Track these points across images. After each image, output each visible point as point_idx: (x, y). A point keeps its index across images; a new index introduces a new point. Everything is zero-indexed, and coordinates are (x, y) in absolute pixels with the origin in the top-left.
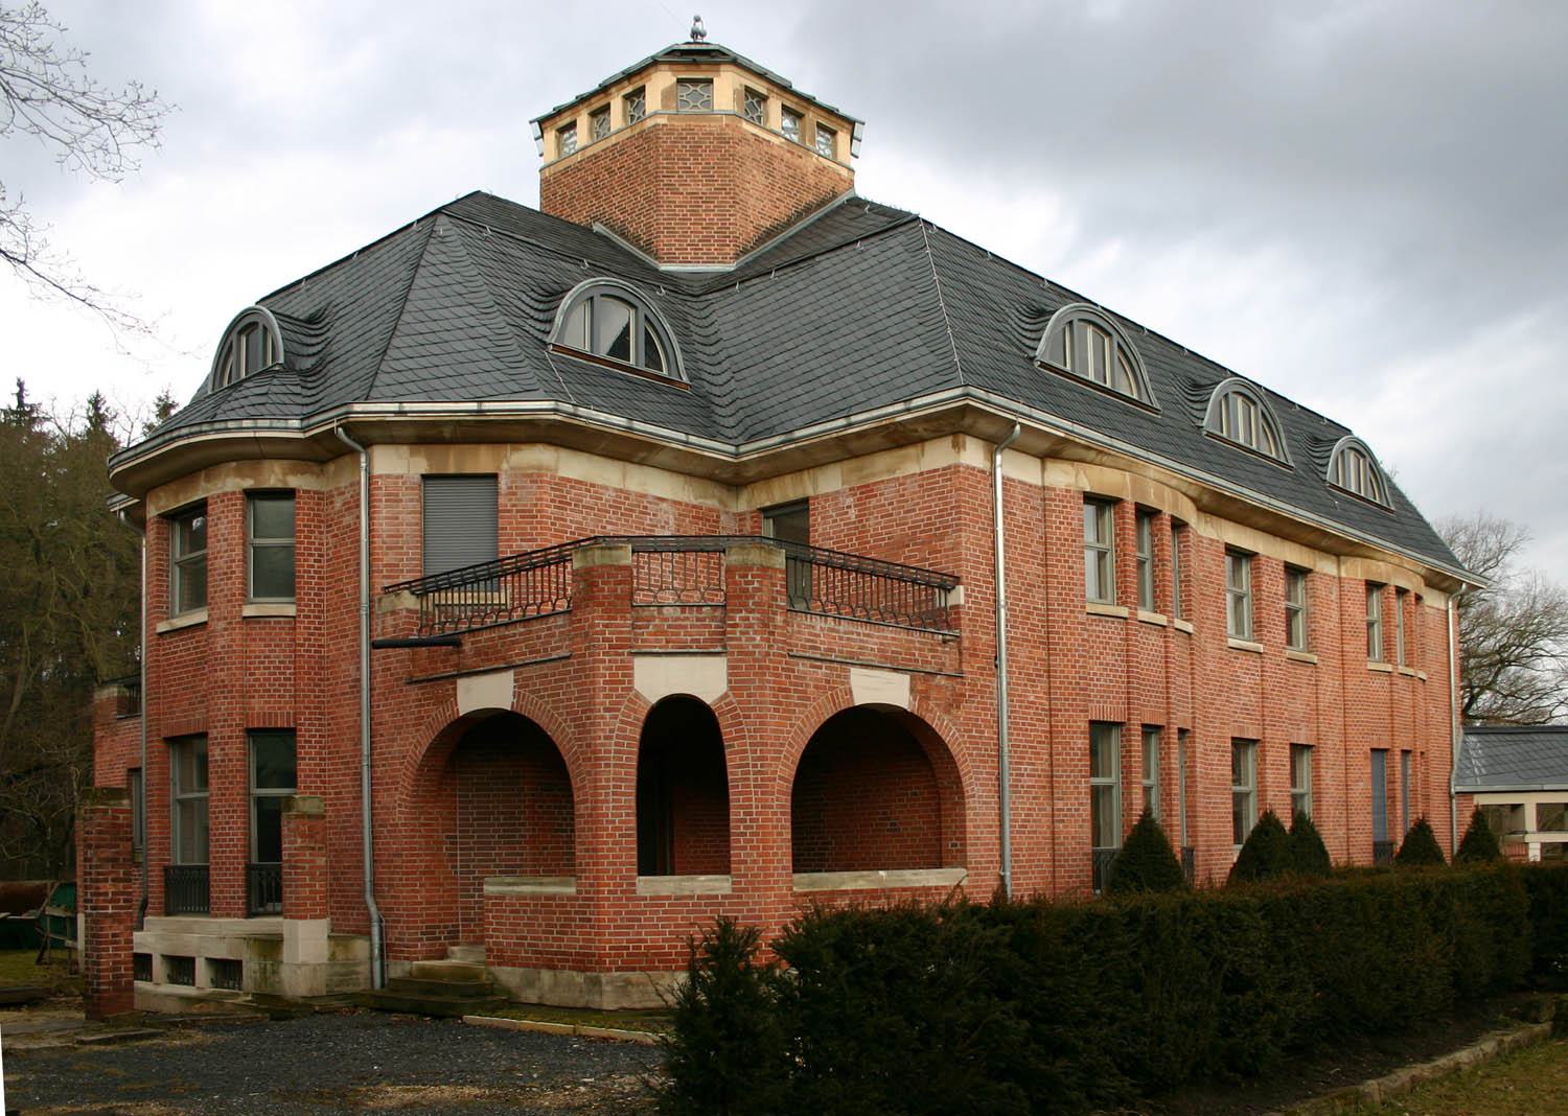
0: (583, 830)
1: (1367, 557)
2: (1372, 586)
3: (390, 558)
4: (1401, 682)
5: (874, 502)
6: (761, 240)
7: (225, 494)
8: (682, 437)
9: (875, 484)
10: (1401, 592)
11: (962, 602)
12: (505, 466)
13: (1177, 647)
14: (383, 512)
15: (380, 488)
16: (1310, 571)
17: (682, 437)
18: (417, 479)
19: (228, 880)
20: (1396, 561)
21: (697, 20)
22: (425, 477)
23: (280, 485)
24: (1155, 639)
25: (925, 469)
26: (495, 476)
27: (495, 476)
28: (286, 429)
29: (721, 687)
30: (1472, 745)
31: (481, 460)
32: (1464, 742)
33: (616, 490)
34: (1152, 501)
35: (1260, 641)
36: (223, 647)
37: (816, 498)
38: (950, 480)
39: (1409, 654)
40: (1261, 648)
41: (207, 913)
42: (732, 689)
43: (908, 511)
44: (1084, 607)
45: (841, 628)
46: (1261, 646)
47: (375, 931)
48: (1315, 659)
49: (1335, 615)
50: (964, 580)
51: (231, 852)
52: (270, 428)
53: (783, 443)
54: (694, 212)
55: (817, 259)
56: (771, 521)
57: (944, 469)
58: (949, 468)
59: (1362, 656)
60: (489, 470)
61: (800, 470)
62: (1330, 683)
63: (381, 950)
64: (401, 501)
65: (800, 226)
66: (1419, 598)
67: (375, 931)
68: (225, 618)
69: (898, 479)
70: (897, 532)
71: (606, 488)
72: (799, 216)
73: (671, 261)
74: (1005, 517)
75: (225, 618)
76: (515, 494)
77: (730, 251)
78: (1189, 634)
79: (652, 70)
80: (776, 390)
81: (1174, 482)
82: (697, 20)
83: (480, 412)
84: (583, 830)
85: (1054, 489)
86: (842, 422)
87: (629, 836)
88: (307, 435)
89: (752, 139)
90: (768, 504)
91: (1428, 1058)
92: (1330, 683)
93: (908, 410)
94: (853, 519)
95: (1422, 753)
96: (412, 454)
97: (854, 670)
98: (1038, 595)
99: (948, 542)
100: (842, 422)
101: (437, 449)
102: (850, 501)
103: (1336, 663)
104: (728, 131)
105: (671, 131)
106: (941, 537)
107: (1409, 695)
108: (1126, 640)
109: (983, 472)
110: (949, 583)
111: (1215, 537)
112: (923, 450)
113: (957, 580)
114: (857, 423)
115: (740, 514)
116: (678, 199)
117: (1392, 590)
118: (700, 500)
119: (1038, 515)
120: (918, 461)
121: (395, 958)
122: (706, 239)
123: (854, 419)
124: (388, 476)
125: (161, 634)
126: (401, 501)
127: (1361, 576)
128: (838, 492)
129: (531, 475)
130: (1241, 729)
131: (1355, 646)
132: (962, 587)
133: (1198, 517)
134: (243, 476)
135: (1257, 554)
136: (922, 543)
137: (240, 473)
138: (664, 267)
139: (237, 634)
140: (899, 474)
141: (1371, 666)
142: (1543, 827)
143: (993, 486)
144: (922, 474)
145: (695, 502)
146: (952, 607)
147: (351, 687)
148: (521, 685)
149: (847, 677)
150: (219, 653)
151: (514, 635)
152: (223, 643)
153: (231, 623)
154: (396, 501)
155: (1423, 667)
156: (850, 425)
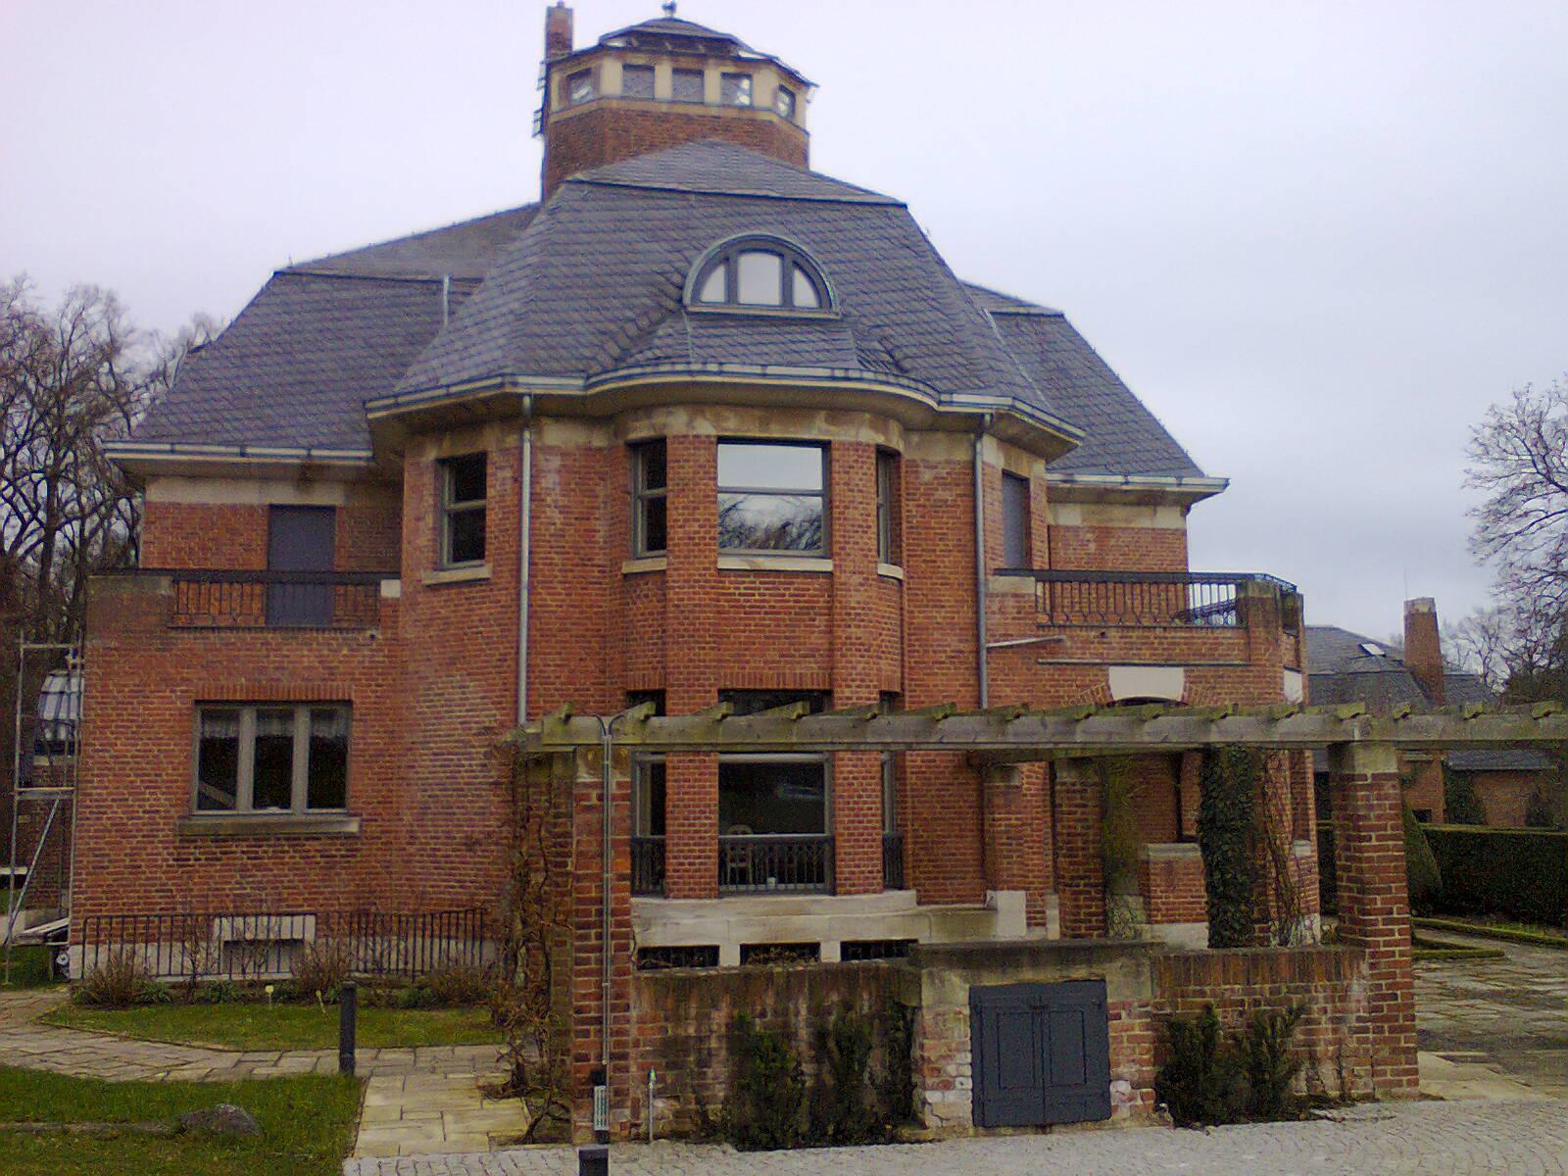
5: (1112, 542)
7: (859, 444)
19: (866, 853)
41: (663, 894)
51: (869, 822)
53: (1065, 482)
69: (1133, 529)
75: (861, 573)
79: (763, 66)
80: (502, 320)
88: (942, 409)
91: (1021, 985)
94: (1093, 551)
101: (1014, 451)
102: (1089, 536)
112: (1155, 514)
140: (1133, 525)
142: (285, 802)
148: (1191, 680)
152: (860, 599)
156: (1127, 483)
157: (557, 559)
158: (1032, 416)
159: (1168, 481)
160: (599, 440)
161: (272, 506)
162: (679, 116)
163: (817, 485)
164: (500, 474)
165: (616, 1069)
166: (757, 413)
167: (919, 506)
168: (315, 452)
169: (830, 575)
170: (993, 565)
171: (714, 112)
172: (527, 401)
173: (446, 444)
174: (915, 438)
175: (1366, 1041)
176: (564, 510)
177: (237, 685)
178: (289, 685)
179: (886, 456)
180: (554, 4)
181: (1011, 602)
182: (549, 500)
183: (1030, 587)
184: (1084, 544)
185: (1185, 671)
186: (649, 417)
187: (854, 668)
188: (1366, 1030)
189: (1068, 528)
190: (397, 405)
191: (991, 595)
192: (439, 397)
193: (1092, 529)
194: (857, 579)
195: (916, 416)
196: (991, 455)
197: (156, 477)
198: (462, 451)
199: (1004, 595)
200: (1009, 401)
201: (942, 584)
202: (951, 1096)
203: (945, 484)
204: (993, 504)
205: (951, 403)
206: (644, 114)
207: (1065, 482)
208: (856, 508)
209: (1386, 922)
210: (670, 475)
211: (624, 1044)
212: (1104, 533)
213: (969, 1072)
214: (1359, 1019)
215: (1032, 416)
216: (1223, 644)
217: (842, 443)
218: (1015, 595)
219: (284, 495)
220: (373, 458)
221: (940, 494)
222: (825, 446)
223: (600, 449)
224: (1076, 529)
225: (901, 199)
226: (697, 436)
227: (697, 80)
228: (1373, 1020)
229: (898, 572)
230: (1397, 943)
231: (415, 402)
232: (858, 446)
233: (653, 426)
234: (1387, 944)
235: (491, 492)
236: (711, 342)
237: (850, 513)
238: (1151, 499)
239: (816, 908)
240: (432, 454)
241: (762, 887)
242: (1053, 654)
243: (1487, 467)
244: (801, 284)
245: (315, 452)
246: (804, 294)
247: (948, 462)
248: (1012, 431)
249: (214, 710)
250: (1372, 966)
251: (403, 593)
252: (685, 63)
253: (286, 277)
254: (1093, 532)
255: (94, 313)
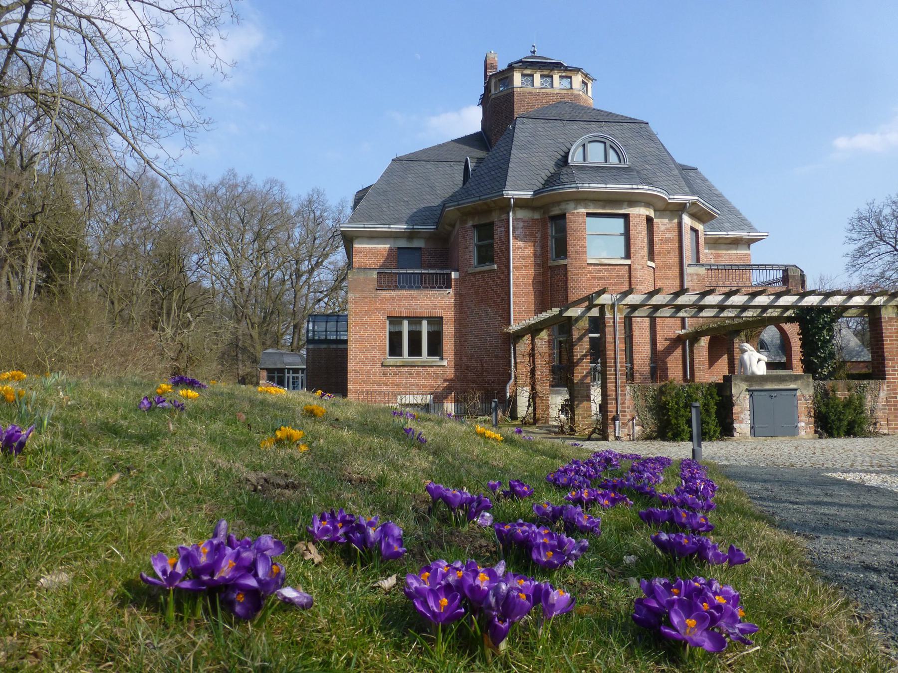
158: (703, 204)
159: (744, 234)
160: (537, 216)
161: (398, 248)
163: (622, 231)
164: (500, 229)
165: (622, 415)
166: (601, 203)
168: (415, 227)
169: (630, 266)
170: (688, 263)
171: (557, 91)
173: (476, 219)
174: (658, 213)
175: (885, 413)
177: (402, 311)
178: (419, 311)
179: (649, 220)
183: (702, 271)
186: (559, 206)
188: (885, 409)
190: (459, 205)
191: (687, 274)
192: (476, 201)
194: (640, 267)
195: (660, 205)
196: (687, 220)
197: (357, 237)
198: (483, 222)
199: (693, 274)
200: (696, 198)
202: (743, 426)
204: (687, 237)
206: (530, 93)
209: (892, 371)
211: (625, 407)
213: (749, 417)
214: (883, 405)
215: (703, 204)
217: (634, 214)
218: (696, 274)
219: (403, 244)
220: (437, 229)
222: (626, 217)
223: (537, 219)
225: (646, 121)
227: (549, 80)
228: (887, 405)
229: (653, 264)
231: (467, 203)
233: (561, 209)
234: (893, 378)
235: (496, 237)
238: (736, 242)
240: (470, 223)
243: (855, 235)
244: (611, 153)
245: (415, 227)
246: (613, 158)
248: (695, 210)
249: (394, 320)
250: (888, 386)
251: (460, 276)
252: (546, 72)
253: (396, 160)
255: (275, 190)
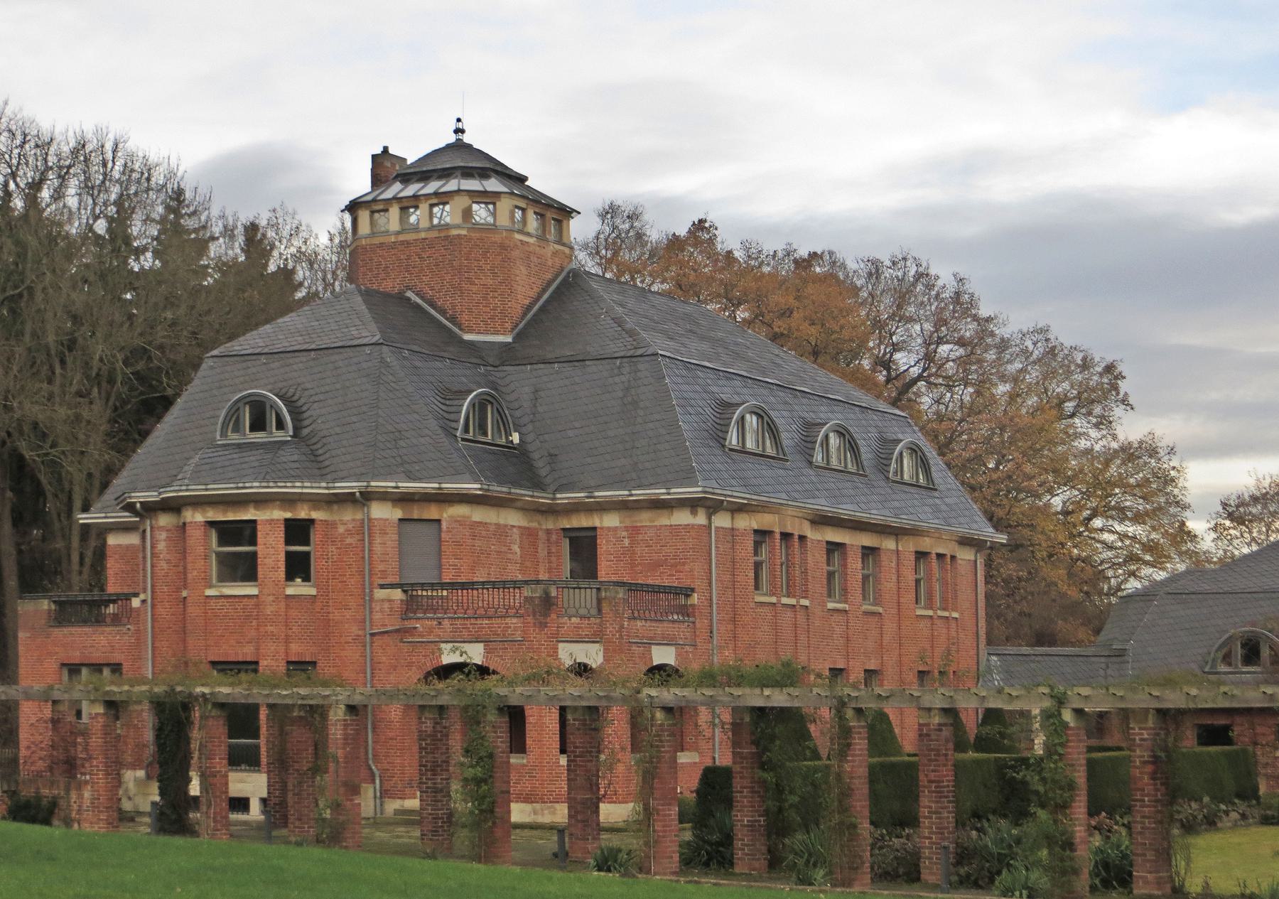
0: (531, 730)
1: (917, 535)
2: (921, 555)
3: (381, 567)
4: (938, 622)
5: (640, 537)
6: (525, 314)
7: (272, 520)
8: (531, 493)
9: (642, 526)
10: (940, 556)
11: (696, 603)
12: (445, 515)
13: (801, 618)
14: (378, 540)
15: (376, 526)
16: (878, 549)
17: (531, 493)
18: (397, 522)
20: (937, 535)
21: (459, 120)
22: (400, 520)
23: (307, 517)
24: (789, 614)
25: (673, 523)
26: (439, 521)
27: (439, 521)
28: (320, 488)
29: (600, 660)
30: (993, 663)
31: (432, 512)
32: (988, 660)
33: (496, 524)
34: (789, 530)
35: (846, 602)
36: (272, 612)
37: (602, 528)
38: (689, 532)
39: (944, 599)
40: (847, 607)
42: (604, 660)
43: (662, 546)
44: (753, 599)
45: (647, 625)
46: (847, 606)
47: (378, 781)
48: (881, 610)
49: (894, 578)
50: (696, 590)
52: (312, 487)
53: (587, 497)
54: (485, 298)
55: (587, 363)
56: (568, 540)
57: (686, 525)
58: (688, 525)
59: (912, 606)
60: (437, 518)
61: (591, 510)
62: (890, 627)
63: (381, 793)
64: (387, 534)
65: (545, 297)
66: (953, 558)
67: (378, 781)
68: (274, 595)
69: (656, 526)
70: (655, 556)
71: (490, 524)
72: (544, 291)
73: (470, 331)
74: (716, 557)
76: (451, 532)
77: (508, 326)
78: (807, 607)
81: (800, 515)
82: (459, 120)
83: (440, 489)
84: (531, 730)
85: (738, 530)
86: (626, 493)
87: (556, 734)
89: (519, 243)
90: (568, 526)
92: (890, 627)
93: (669, 494)
95: (954, 672)
96: (393, 507)
97: (653, 647)
98: (730, 592)
99: (687, 568)
100: (626, 493)
102: (624, 534)
103: (894, 611)
104: (507, 242)
105: (469, 239)
106: (684, 564)
107: (944, 631)
108: (775, 616)
109: (704, 526)
110: (688, 592)
111: (821, 539)
113: (693, 590)
114: (635, 495)
115: (548, 530)
116: (475, 289)
117: (934, 556)
118: (531, 524)
119: (730, 545)
120: (670, 519)
121: (389, 798)
122: (492, 318)
123: (634, 492)
124: (381, 519)
125: (207, 597)
126: (387, 534)
127: (912, 549)
128: (616, 527)
129: (458, 521)
130: (835, 662)
131: (909, 597)
132: (696, 595)
133: (812, 527)
134: (285, 510)
135: (845, 544)
136: (671, 566)
137: (283, 509)
138: (467, 337)
139: (283, 605)
140: (655, 524)
141: (919, 612)
143: (710, 534)
144: (671, 526)
145: (527, 525)
146: (691, 605)
147: (353, 639)
149: (650, 651)
150: (269, 615)
151: (482, 624)
153: (277, 598)
154: (385, 533)
155: (955, 610)
156: (631, 495)
157: (166, 589)
162: (402, 243)
167: (337, 548)
172: (138, 505)
176: (168, 562)
180: (379, 151)
181: (386, 605)
182: (161, 556)
184: (620, 540)
185: (485, 646)
187: (269, 649)
189: (609, 529)
193: (626, 528)
194: (271, 598)
199: (383, 600)
201: (350, 595)
203: (352, 534)
205: (334, 488)
207: (587, 497)
208: (270, 558)
210: (283, 526)
212: (634, 531)
216: (510, 627)
217: (262, 520)
221: (349, 541)
224: (615, 529)
226: (195, 522)
230: (100, 779)
232: (271, 521)
234: (98, 779)
236: (247, 459)
237: (267, 561)
239: (249, 779)
241: (239, 768)
242: (412, 635)
247: (353, 520)
250: (92, 787)
254: (627, 531)
